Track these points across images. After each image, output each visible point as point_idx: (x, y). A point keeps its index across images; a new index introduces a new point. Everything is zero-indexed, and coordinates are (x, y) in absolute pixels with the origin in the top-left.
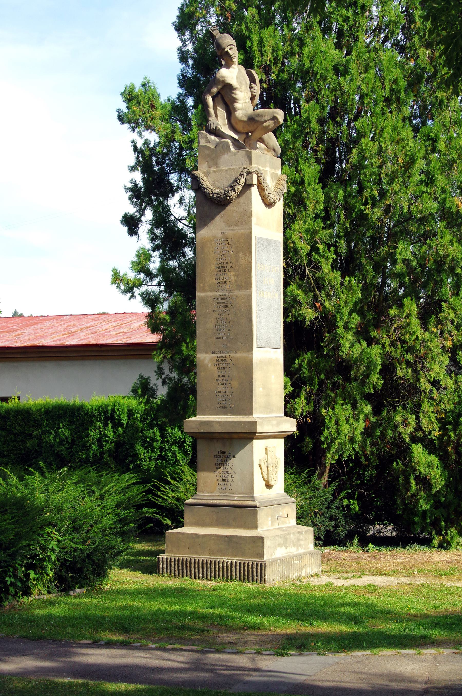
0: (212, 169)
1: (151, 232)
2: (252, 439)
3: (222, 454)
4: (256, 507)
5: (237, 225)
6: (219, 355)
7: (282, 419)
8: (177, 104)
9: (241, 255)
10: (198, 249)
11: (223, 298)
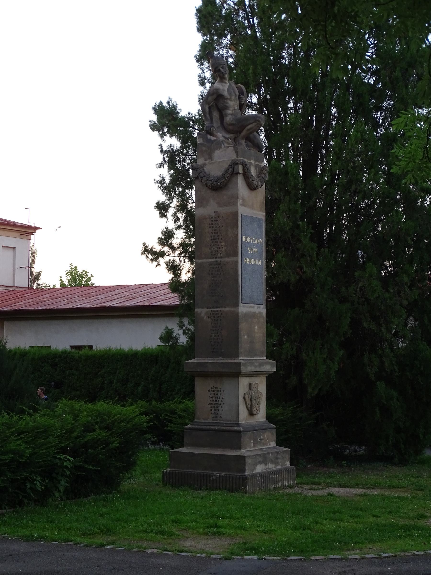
0: (208, 162)
1: (175, 215)
2: (238, 377)
3: (215, 390)
4: (240, 432)
5: (227, 206)
6: (212, 309)
7: (264, 361)
8: (197, 117)
9: (229, 229)
10: (197, 223)
11: (216, 263)
